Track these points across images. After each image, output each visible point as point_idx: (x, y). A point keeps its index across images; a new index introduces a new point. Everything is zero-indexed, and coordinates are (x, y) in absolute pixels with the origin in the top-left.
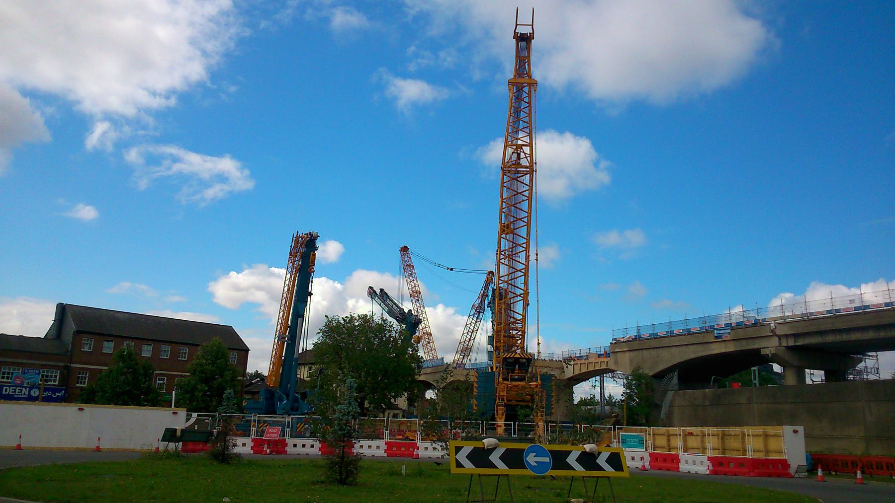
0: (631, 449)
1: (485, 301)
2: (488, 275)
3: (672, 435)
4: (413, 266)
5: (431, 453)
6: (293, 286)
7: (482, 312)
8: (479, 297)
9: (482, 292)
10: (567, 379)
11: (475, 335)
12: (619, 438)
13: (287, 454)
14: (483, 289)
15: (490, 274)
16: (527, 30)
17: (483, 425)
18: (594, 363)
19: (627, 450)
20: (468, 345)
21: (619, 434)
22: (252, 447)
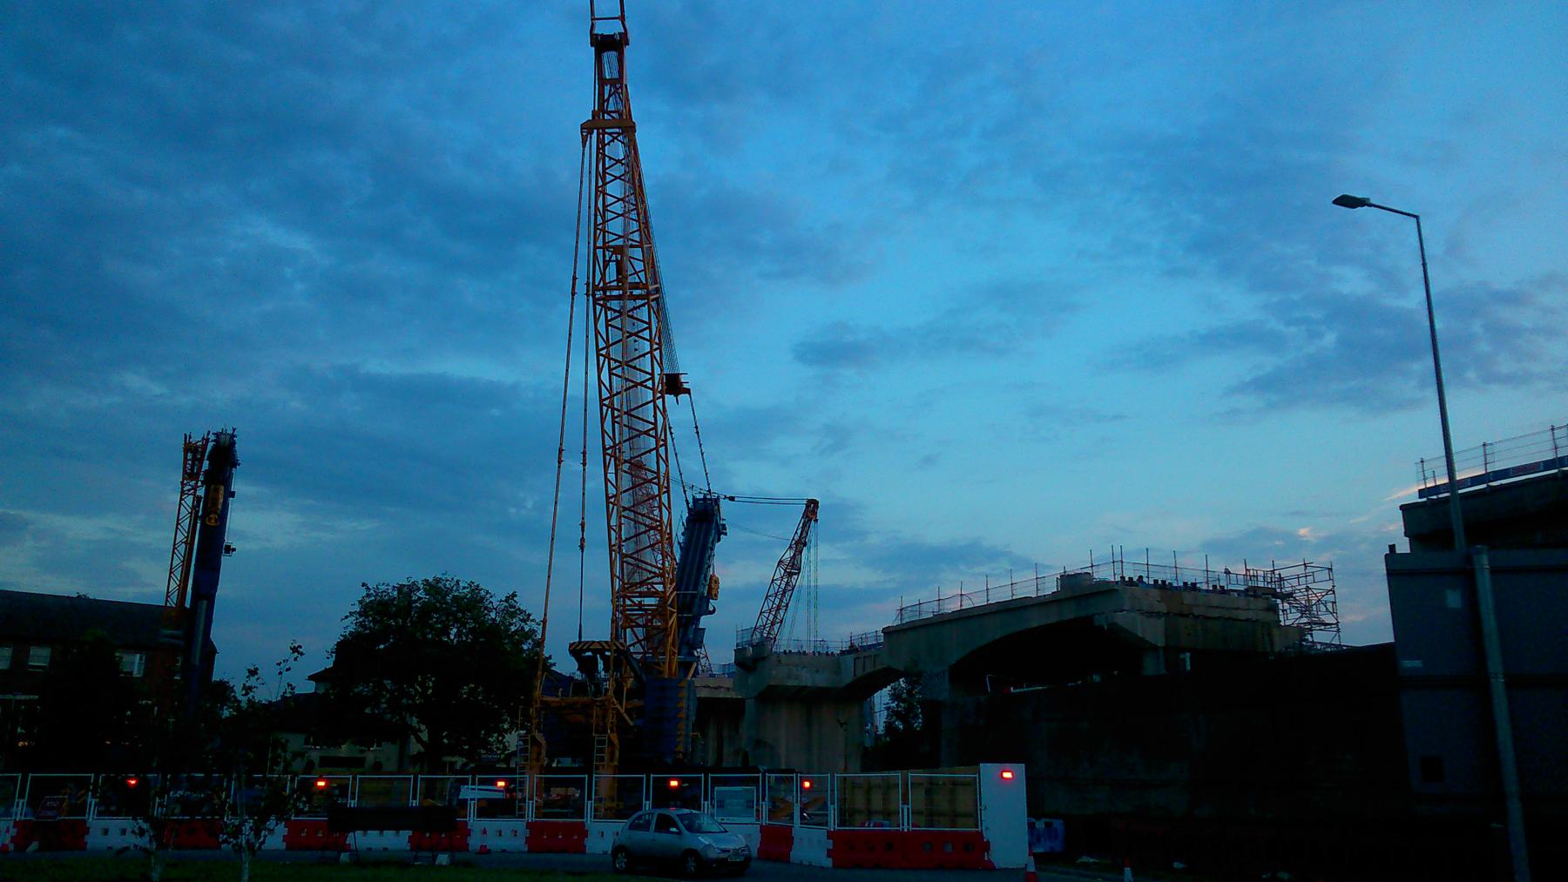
1: (801, 553)
2: (808, 506)
5: (116, 841)
7: (795, 574)
8: (790, 547)
9: (797, 538)
13: (468, 850)
14: (799, 531)
16: (610, 28)
19: (725, 821)
20: (769, 633)
21: (712, 791)
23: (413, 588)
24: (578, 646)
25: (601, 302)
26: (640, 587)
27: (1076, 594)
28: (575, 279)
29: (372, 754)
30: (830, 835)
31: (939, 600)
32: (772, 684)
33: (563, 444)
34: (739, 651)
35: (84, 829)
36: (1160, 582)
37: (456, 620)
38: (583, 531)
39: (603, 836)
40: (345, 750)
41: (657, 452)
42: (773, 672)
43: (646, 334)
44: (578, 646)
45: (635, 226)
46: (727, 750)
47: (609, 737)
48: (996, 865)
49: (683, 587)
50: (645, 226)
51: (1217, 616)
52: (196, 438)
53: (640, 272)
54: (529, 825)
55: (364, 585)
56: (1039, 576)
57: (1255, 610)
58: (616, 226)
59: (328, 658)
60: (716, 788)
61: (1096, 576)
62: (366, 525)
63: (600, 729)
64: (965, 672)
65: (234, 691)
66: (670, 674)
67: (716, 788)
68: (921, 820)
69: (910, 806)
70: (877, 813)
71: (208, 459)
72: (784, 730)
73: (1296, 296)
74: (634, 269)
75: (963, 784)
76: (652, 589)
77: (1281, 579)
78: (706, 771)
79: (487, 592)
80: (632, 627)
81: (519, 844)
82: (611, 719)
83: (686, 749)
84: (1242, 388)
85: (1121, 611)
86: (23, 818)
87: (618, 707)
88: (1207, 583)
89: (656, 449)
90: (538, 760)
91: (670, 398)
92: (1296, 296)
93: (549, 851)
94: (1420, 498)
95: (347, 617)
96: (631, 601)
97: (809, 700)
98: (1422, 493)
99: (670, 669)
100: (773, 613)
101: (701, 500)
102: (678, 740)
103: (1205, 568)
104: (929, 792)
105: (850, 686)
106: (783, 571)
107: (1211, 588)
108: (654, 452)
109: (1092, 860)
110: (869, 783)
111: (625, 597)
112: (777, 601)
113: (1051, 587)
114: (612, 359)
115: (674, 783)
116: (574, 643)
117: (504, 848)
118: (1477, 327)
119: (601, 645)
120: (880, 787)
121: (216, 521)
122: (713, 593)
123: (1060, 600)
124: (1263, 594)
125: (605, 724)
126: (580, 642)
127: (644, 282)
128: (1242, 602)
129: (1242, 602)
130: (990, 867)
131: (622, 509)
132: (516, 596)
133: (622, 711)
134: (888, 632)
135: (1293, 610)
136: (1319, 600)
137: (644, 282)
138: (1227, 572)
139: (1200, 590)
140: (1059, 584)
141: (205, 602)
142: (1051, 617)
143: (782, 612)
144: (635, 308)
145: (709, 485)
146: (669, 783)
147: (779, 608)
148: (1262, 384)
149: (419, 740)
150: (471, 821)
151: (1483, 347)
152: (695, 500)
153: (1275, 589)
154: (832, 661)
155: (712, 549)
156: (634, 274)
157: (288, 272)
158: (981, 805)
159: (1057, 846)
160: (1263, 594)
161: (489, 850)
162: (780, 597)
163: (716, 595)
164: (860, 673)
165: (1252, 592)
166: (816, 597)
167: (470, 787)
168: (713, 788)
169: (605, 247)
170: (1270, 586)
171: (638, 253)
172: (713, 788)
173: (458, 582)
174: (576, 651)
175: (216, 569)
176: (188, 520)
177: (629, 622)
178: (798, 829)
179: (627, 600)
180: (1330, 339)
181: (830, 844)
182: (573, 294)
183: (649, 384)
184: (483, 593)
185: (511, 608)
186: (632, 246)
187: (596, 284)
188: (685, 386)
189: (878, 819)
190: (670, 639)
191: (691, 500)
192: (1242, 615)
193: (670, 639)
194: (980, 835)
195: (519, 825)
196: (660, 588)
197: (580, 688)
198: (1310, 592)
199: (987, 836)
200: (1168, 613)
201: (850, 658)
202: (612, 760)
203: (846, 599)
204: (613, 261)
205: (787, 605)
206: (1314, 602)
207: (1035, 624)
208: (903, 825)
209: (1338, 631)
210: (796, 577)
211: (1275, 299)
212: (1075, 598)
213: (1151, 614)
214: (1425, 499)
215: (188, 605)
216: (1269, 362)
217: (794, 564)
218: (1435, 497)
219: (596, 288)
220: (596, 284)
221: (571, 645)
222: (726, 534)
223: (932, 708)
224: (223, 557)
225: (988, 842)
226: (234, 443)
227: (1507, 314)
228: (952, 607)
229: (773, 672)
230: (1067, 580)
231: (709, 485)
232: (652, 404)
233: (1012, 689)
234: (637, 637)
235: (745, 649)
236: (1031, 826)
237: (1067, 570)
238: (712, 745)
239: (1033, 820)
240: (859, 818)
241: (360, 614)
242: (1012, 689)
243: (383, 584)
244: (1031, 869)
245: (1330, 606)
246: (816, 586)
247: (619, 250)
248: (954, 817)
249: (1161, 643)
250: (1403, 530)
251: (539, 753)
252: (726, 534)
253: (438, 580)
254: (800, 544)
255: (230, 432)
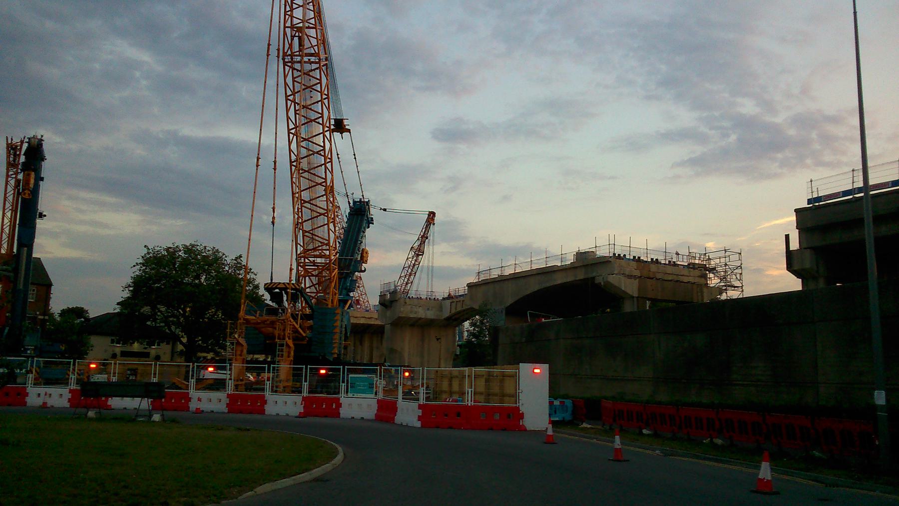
0: (359, 395)
2: (429, 215)
3: (454, 377)
4: (339, 207)
6: (15, 220)
7: (421, 255)
8: (418, 239)
9: (422, 234)
10: (444, 319)
11: (413, 278)
12: (348, 380)
14: (424, 230)
15: (432, 215)
17: (74, 364)
18: (461, 302)
21: (348, 377)
22: (341, 407)
23: (176, 250)
24: (270, 285)
25: (290, 64)
26: (314, 252)
27: (585, 264)
28: (269, 45)
29: (154, 350)
30: (420, 407)
31: (502, 267)
32: (400, 316)
33: (260, 154)
34: (382, 296)
35: (23, 394)
36: (637, 258)
37: (204, 271)
38: (274, 212)
39: (286, 404)
40: (136, 347)
41: (325, 166)
42: (402, 309)
43: (318, 87)
44: (270, 285)
45: (312, 14)
46: (375, 353)
47: (286, 342)
48: (527, 428)
49: (345, 254)
50: (318, 14)
51: (670, 279)
52: (16, 140)
53: (314, 46)
54: (229, 396)
55: (145, 246)
56: (563, 253)
57: (692, 277)
58: (298, 13)
59: (123, 291)
60: (350, 376)
61: (597, 253)
62: (180, 222)
63: (281, 337)
64: (516, 310)
65: (88, 313)
66: (333, 306)
67: (350, 376)
68: (481, 398)
69: (473, 390)
70: (455, 393)
71: (24, 155)
72: (407, 344)
73: (716, 114)
74: (312, 45)
75: (510, 377)
76: (323, 254)
77: (709, 259)
78: (344, 365)
79: (224, 254)
80: (309, 276)
81: (222, 407)
82: (288, 331)
83: (340, 351)
84: (682, 164)
85: (612, 275)
86: (473, 404)
87: (294, 323)
88: (665, 259)
89: (325, 164)
90: (241, 355)
91: (337, 135)
92: (716, 114)
93: (241, 412)
94: (808, 204)
95: (134, 266)
96: (309, 260)
97: (422, 326)
98: (809, 201)
99: (332, 302)
100: (407, 277)
101: (358, 202)
102: (334, 346)
103: (664, 251)
104: (487, 381)
105: (448, 319)
106: (413, 253)
107: (667, 263)
108: (323, 166)
109: (589, 426)
110: (451, 374)
111: (305, 258)
112: (410, 270)
113: (570, 260)
114: (297, 103)
115: (323, 372)
116: (268, 283)
117: (126, 407)
118: (814, 135)
119: (285, 285)
120: (457, 377)
121: (29, 194)
122: (365, 259)
123: (576, 268)
124: (699, 267)
125: (285, 335)
126: (271, 283)
127: (317, 52)
128: (686, 272)
129: (686, 272)
130: (523, 429)
131: (303, 202)
132: (242, 257)
133: (297, 326)
134: (470, 286)
135: (716, 278)
136: (732, 272)
137: (317, 52)
138: (677, 254)
139: (660, 263)
140: (575, 258)
141: (26, 248)
142: (569, 278)
143: (412, 277)
144: (312, 70)
145: (362, 192)
146: (320, 372)
147: (410, 275)
148: (694, 162)
149: (182, 343)
150: (267, 395)
151: (817, 146)
152: (355, 202)
153: (706, 265)
154: (438, 304)
155: (364, 232)
156: (311, 47)
157: (138, 74)
158: (519, 390)
159: (568, 416)
160: (699, 267)
161: (203, 411)
162: (411, 268)
163: (366, 261)
164: (453, 311)
165: (692, 266)
166: (431, 271)
167: (425, 391)
168: (348, 375)
169: (292, 27)
170: (702, 263)
171: (312, 32)
172: (348, 375)
173: (205, 247)
174: (269, 288)
175: (33, 228)
176: (12, 196)
177: (307, 274)
178: (401, 403)
179: (306, 259)
180: (733, 137)
181: (420, 412)
182: (268, 55)
183: (320, 120)
184: (221, 254)
185: (238, 264)
186: (309, 28)
187: (286, 51)
188: (347, 127)
189: (456, 397)
190: (333, 284)
191: (351, 202)
192: (686, 279)
193: (333, 284)
194: (518, 409)
195: (298, 398)
196: (327, 253)
197: (272, 311)
198: (727, 267)
199: (522, 409)
200: (641, 277)
201: (448, 302)
202: (289, 357)
203: (450, 274)
204: (297, 36)
205: (416, 273)
206: (729, 273)
207: (559, 282)
208: (468, 401)
209: (742, 291)
210: (421, 257)
211: (705, 114)
212: (584, 266)
213: (630, 277)
214: (811, 205)
215: (15, 250)
216: (698, 150)
217: (420, 249)
218: (817, 204)
219: (285, 54)
220: (286, 51)
221: (265, 284)
222: (373, 224)
223: (495, 332)
224: (37, 220)
225: (523, 414)
226: (41, 145)
227: (832, 129)
228: (508, 272)
229: (402, 309)
230: (580, 255)
231: (362, 192)
232: (322, 135)
233: (543, 319)
234: (312, 283)
235: (385, 295)
236: (551, 403)
237: (580, 249)
238: (366, 351)
239: (552, 399)
240: (444, 396)
241: (143, 264)
242: (543, 319)
243: (158, 246)
244: (550, 432)
245: (738, 276)
246: (432, 267)
247: (300, 30)
248: (503, 396)
249: (636, 294)
250: (796, 225)
251: (242, 351)
252: (373, 224)
253: (193, 246)
254: (424, 238)
255: (39, 137)
